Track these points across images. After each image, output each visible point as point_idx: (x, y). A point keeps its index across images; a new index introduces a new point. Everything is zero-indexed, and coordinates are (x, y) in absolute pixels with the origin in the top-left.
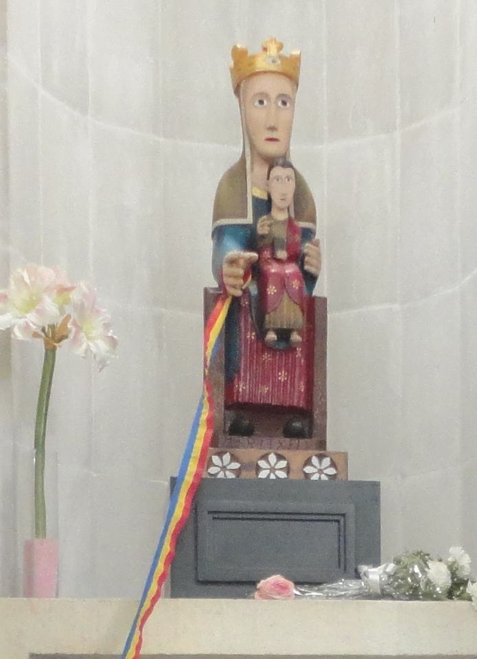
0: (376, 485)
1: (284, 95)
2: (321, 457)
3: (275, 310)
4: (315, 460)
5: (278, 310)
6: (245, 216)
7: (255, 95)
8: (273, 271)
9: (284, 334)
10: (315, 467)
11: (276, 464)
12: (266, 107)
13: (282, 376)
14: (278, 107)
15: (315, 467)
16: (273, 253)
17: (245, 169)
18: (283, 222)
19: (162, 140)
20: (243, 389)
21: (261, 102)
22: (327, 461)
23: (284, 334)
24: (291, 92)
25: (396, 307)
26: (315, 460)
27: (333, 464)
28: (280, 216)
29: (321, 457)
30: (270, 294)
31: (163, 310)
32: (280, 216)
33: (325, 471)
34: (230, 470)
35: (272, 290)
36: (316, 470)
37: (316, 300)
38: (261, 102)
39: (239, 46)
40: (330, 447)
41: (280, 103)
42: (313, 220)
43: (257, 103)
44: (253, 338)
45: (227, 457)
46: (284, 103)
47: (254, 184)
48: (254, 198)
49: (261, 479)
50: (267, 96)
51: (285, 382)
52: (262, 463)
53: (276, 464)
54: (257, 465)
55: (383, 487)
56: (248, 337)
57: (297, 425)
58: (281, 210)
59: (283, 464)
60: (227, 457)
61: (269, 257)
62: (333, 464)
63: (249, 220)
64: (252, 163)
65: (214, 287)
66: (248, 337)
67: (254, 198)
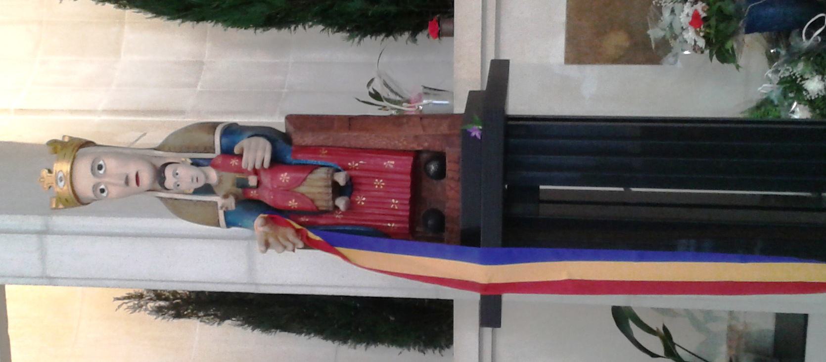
1: (92, 170)
3: (313, 201)
5: (200, 184)
9: (337, 190)
12: (106, 187)
16: (252, 188)
21: (102, 191)
23: (337, 190)
28: (213, 175)
30: (375, 181)
37: (500, 242)
38: (102, 191)
41: (101, 172)
43: (104, 194)
44: (397, 202)
50: (175, 183)
51: (385, 180)
55: (511, 62)
57: (433, 168)
61: (255, 192)
65: (393, 38)
66: (393, 201)
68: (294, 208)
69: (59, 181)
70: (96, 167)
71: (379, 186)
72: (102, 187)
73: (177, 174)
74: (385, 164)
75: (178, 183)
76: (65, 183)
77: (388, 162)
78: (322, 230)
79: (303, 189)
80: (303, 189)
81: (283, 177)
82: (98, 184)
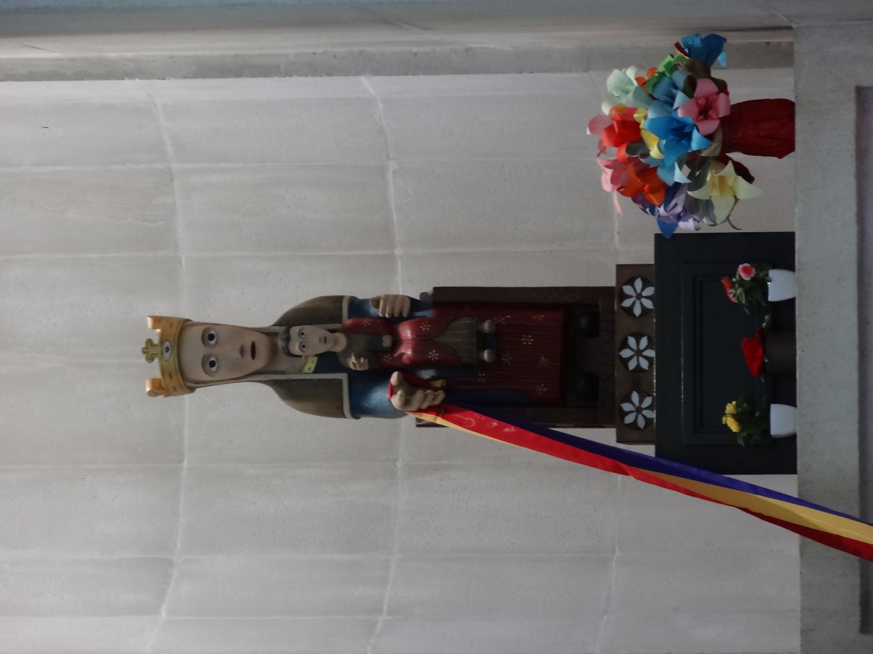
0: (655, 234)
2: (623, 296)
4: (627, 303)
6: (339, 382)
7: (302, 351)
8: (409, 352)
9: (483, 341)
10: (634, 303)
11: (632, 349)
12: (216, 359)
13: (528, 340)
14: (217, 342)
15: (634, 303)
17: (286, 381)
18: (349, 340)
19: (185, 464)
20: (544, 387)
22: (627, 289)
23: (483, 341)
24: (414, 320)
25: (393, 165)
26: (627, 303)
27: (631, 282)
29: (623, 296)
31: (399, 465)
32: (340, 343)
33: (639, 290)
34: (643, 290)
35: (433, 355)
36: (638, 302)
39: (148, 389)
40: (611, 281)
41: (213, 342)
42: (339, 299)
44: (484, 375)
45: (626, 407)
46: (211, 337)
47: (300, 371)
48: (316, 371)
49: (654, 305)
52: (632, 365)
53: (632, 349)
54: (634, 371)
56: (483, 380)
57: (584, 322)
58: (336, 342)
59: (632, 341)
60: (626, 407)
62: (631, 282)
63: (343, 377)
64: (276, 373)
67: (316, 371)
68: (435, 359)
69: (164, 351)
70: (207, 336)
71: (527, 342)
72: (213, 359)
73: (303, 334)
74: (534, 317)
75: (304, 344)
76: (171, 354)
77: (538, 316)
78: (670, 211)
79: (444, 339)
80: (444, 339)
81: (426, 328)
82: (210, 356)
